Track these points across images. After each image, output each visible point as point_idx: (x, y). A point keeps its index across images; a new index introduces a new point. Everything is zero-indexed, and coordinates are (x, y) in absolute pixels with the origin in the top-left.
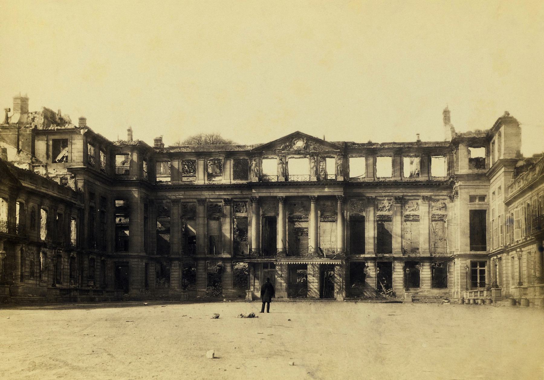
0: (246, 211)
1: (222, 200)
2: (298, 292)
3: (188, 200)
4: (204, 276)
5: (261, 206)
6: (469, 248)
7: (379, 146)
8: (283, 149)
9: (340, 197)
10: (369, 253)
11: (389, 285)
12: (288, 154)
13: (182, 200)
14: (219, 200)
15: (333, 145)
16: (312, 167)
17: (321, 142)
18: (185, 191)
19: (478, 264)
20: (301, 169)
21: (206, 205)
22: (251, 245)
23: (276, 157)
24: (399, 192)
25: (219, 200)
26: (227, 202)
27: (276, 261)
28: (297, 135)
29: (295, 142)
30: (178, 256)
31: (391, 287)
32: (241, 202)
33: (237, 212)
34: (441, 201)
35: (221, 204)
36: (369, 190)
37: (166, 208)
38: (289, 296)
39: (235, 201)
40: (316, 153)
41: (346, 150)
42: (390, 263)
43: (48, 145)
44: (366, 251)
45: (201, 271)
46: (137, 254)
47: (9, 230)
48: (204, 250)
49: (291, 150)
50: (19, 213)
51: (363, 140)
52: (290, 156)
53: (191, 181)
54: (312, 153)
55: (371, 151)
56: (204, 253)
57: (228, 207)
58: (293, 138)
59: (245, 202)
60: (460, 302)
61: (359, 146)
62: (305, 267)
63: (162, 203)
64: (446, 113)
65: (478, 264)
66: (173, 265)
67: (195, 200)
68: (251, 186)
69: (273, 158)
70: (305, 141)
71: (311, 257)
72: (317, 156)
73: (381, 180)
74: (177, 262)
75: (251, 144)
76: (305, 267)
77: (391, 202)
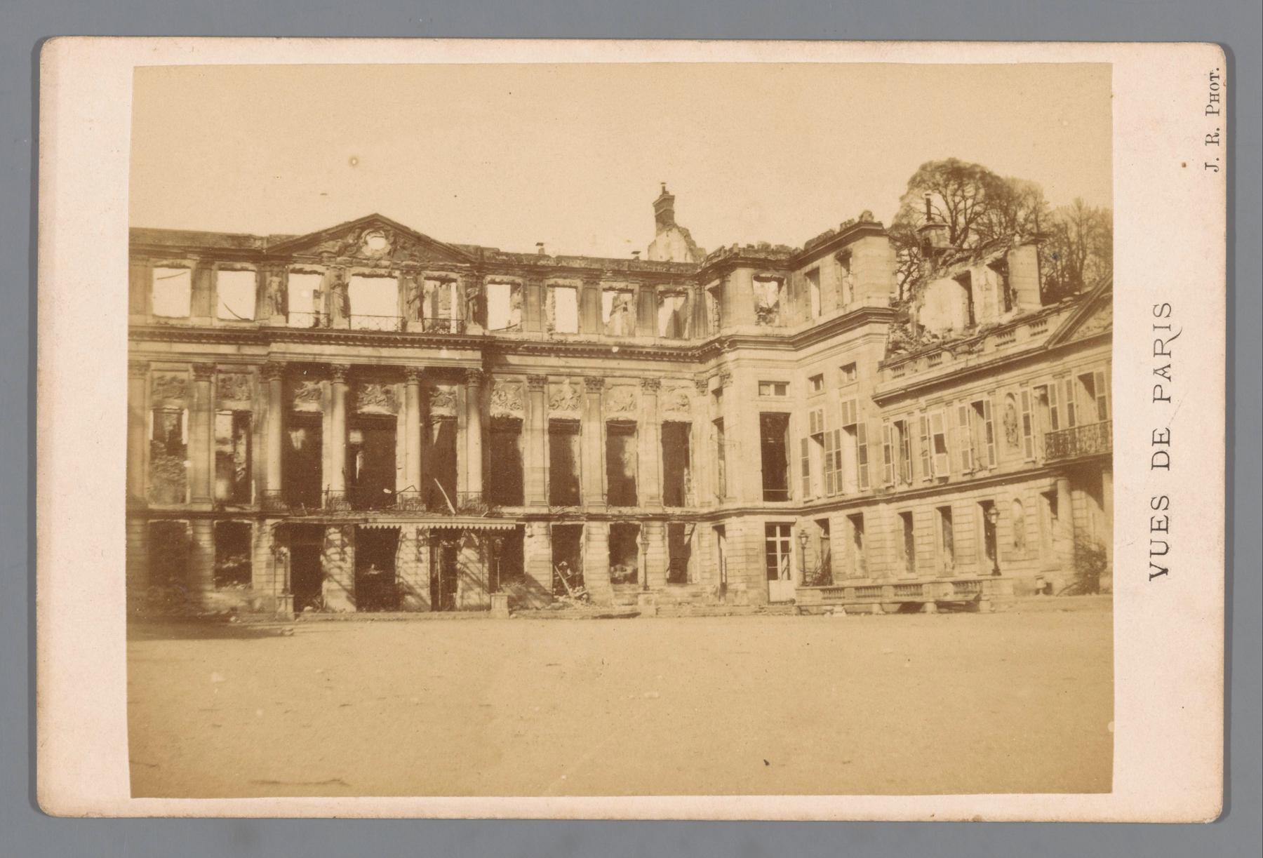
0: (249, 398)
1: (190, 366)
2: (377, 592)
7: (552, 263)
8: (339, 254)
10: (533, 504)
11: (577, 581)
12: (351, 265)
15: (453, 253)
16: (412, 298)
17: (422, 241)
18: (350, 331)
19: (778, 529)
20: (376, 302)
22: (262, 480)
23: (251, 267)
24: (593, 366)
26: (203, 371)
28: (373, 223)
29: (368, 238)
31: (581, 583)
33: (226, 396)
34: (677, 392)
35: (184, 376)
36: (1071, 318)
38: (360, 606)
39: (220, 371)
41: (479, 266)
42: (577, 530)
44: (527, 500)
51: (526, 247)
52: (429, 273)
54: (407, 266)
55: (533, 273)
58: (363, 229)
60: (1076, 503)
65: (778, 529)
69: (243, 269)
70: (392, 239)
71: (405, 510)
77: (578, 388)
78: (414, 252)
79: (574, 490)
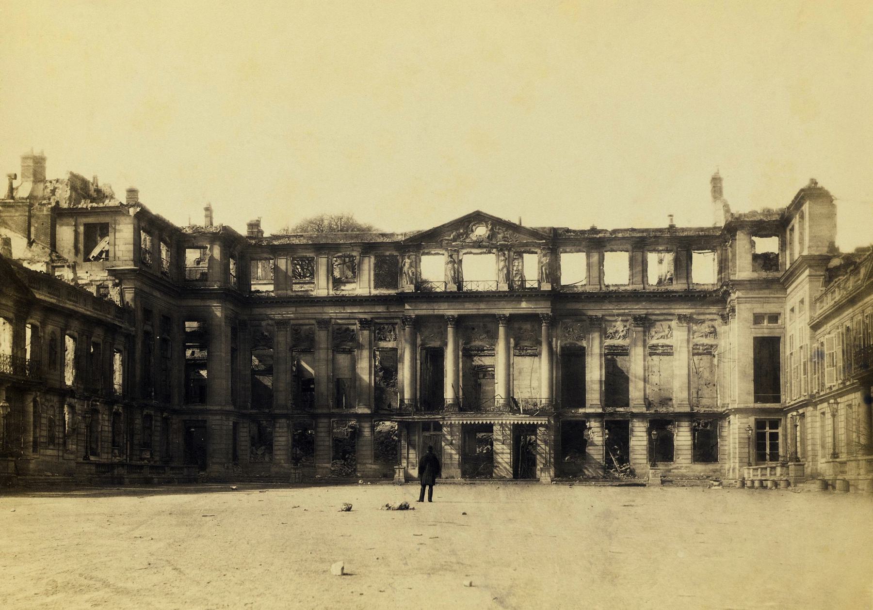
0: (395, 339)
1: (357, 322)
2: (478, 468)
3: (301, 322)
4: (327, 443)
5: (420, 331)
6: (752, 398)
7: (608, 235)
8: (454, 240)
9: (545, 317)
10: (592, 406)
11: (624, 458)
12: (463, 247)
13: (292, 322)
14: (352, 321)
15: (534, 233)
16: (501, 267)
17: (516, 228)
18: (296, 307)
20: (482, 272)
21: (330, 329)
22: (402, 393)
23: (443, 252)
24: (640, 309)
25: (352, 321)
26: (365, 324)
27: (443, 418)
28: (477, 217)
29: (474, 228)
30: (285, 412)
31: (628, 461)
32: (387, 324)
33: (381, 340)
34: (707, 323)
35: (354, 327)
36: (592, 306)
37: (266, 334)
38: (464, 475)
39: (376, 323)
40: (507, 245)
41: (555, 241)
42: (627, 423)
43: (76, 232)
44: (588, 403)
45: (323, 434)
46: (220, 407)
47: (15, 370)
48: (328, 401)
49: (468, 240)
50: (31, 343)
51: (583, 225)
52: (465, 251)
53: (307, 291)
54: (501, 245)
55: (595, 242)
56: (328, 407)
57: (366, 333)
58: (470, 222)
59: (394, 324)
61: (577, 235)
62: (489, 428)
63: (260, 325)
64: (716, 181)
66: (278, 425)
67: (313, 322)
68: (402, 299)
69: (438, 254)
70: (490, 227)
71: (499, 412)
72: (509, 250)
73: (611, 288)
74: (283, 420)
75: (403, 231)
76: (489, 428)
77: (628, 324)
78: (508, 238)
79: (360, 482)
